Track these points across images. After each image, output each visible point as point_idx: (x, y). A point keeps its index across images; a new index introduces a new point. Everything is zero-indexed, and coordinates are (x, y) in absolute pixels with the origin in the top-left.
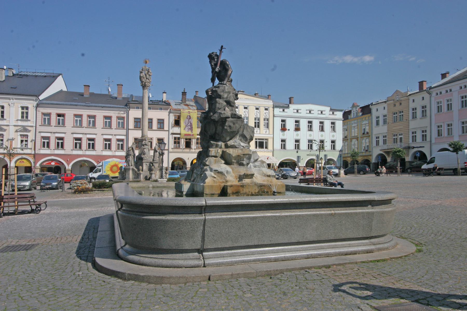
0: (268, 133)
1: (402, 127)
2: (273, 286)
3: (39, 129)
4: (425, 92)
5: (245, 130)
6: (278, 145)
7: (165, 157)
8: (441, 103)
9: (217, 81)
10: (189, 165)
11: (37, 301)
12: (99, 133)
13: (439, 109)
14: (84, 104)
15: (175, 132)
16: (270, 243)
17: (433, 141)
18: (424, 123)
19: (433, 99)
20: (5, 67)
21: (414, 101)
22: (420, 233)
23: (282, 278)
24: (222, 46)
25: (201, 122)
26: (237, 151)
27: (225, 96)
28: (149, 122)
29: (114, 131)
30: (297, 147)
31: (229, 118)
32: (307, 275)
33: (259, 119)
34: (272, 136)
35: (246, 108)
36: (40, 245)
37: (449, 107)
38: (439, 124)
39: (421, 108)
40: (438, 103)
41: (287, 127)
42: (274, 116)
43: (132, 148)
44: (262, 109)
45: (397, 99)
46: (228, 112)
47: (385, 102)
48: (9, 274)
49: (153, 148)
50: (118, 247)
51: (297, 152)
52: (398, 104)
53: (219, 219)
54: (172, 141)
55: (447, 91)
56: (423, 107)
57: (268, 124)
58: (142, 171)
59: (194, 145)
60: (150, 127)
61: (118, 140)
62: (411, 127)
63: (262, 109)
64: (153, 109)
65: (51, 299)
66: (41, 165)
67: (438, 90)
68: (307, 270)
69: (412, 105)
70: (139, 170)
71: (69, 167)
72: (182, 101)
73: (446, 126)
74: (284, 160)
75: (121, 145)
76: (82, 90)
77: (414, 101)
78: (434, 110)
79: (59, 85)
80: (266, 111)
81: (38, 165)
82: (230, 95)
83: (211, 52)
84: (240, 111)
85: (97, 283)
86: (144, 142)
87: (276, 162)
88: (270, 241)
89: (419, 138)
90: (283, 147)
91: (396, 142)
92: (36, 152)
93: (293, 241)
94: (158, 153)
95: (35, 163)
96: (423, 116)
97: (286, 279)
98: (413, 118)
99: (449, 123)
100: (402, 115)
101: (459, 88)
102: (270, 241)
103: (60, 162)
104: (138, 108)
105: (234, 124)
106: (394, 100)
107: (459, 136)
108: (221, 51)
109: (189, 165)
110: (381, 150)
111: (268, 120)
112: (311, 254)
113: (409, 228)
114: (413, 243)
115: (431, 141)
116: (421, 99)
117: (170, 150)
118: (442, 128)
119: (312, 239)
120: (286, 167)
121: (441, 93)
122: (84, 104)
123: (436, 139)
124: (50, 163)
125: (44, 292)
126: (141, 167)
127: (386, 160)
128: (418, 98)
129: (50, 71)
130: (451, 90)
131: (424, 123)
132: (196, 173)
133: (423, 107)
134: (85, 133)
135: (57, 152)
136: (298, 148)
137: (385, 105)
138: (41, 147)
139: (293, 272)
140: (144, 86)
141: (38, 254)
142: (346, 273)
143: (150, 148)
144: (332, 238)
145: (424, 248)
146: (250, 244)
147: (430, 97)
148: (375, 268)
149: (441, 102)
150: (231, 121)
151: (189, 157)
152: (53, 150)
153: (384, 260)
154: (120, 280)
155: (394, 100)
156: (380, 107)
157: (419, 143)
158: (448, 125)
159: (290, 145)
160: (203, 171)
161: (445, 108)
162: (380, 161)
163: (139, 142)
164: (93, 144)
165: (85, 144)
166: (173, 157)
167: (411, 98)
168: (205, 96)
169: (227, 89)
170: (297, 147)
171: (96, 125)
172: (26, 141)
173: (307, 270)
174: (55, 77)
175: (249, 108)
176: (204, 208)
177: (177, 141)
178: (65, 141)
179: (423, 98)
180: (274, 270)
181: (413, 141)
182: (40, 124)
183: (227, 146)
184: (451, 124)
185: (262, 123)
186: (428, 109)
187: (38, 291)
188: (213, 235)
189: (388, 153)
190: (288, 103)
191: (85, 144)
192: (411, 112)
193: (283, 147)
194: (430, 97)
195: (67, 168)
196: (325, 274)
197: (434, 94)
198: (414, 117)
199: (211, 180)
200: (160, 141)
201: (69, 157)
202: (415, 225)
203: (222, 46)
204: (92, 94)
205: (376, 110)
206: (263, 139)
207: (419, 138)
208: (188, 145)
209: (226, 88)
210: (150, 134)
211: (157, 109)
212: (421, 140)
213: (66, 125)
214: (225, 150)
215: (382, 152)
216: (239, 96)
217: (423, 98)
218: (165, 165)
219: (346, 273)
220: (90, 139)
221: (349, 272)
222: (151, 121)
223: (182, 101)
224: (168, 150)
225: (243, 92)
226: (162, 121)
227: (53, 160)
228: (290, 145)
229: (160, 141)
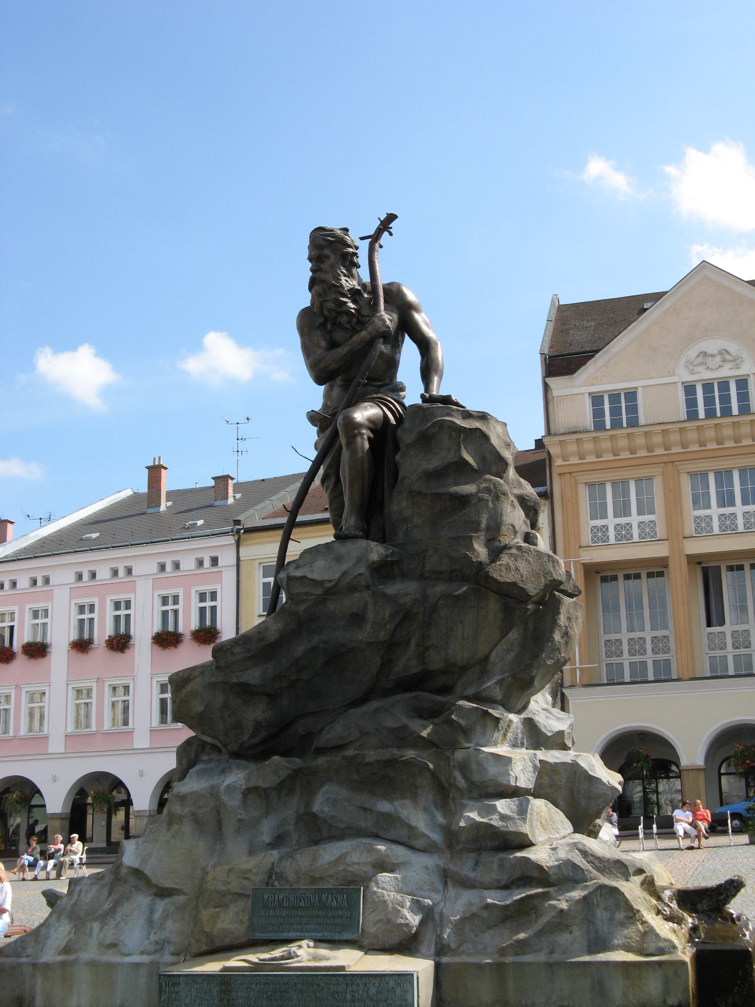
101: (154, 568)
130: (47, 580)
149: (12, 614)
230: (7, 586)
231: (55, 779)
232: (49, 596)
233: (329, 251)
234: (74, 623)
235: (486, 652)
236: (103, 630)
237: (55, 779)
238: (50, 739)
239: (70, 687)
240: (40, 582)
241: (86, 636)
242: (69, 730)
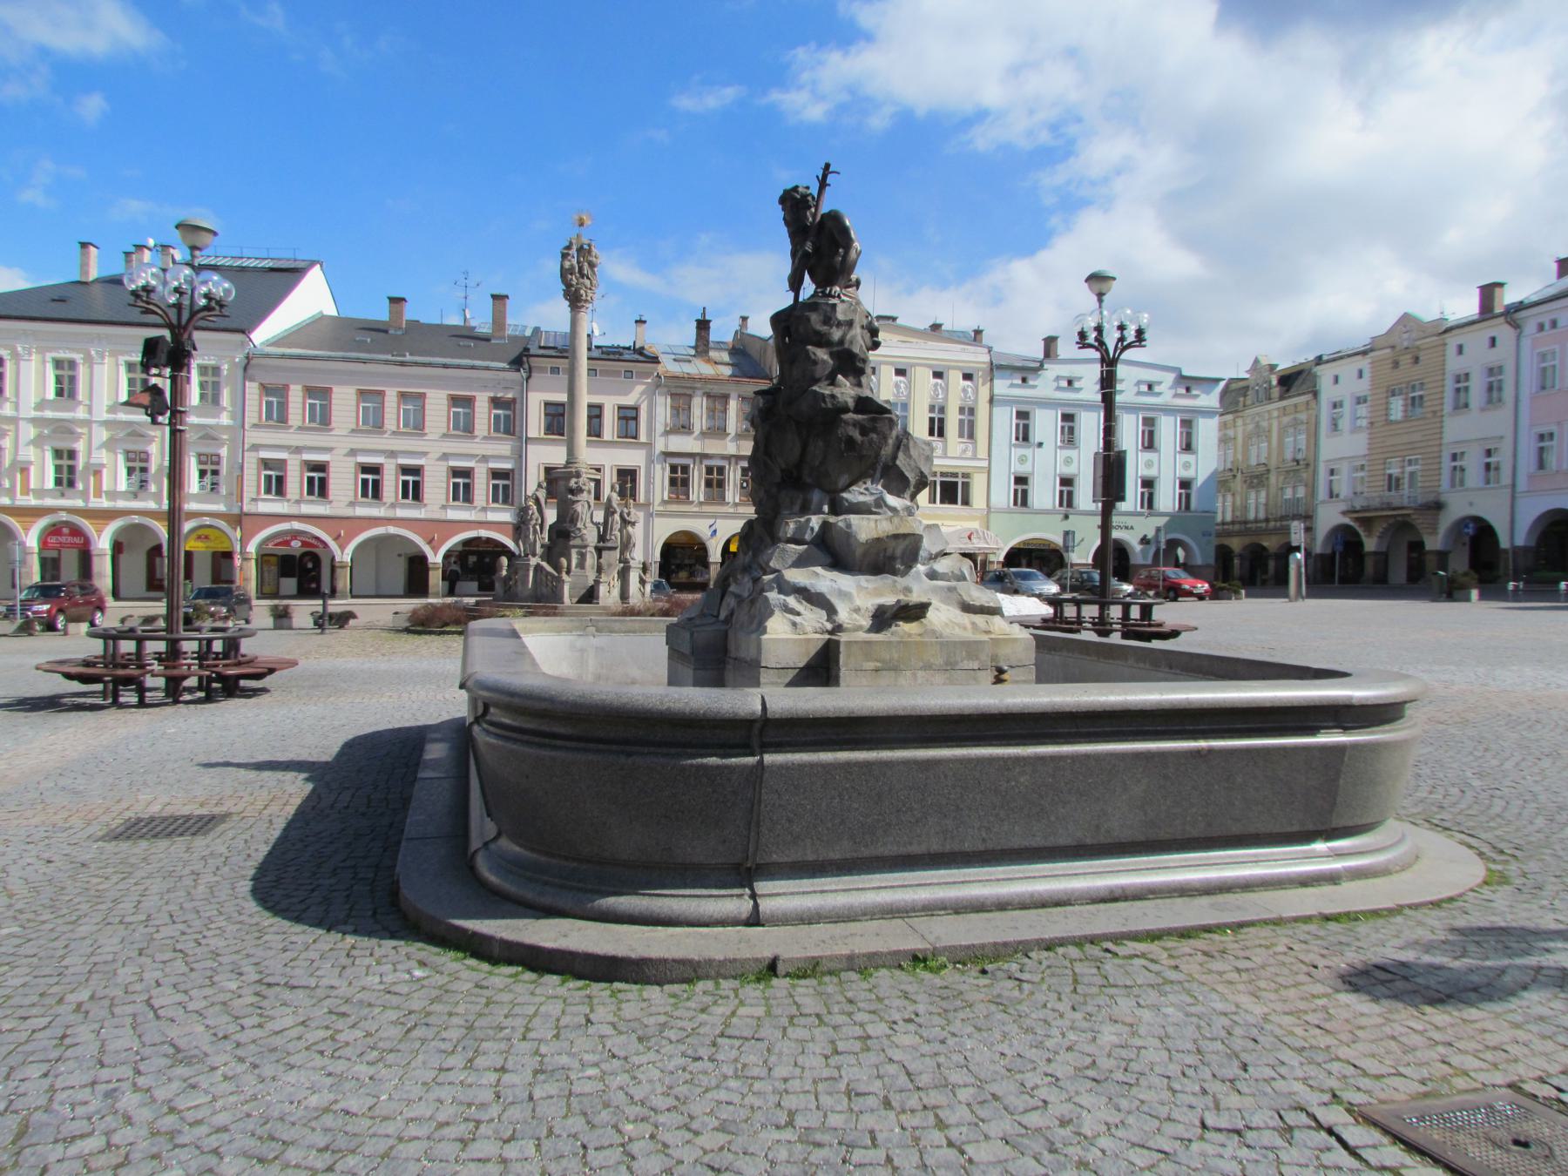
0: (969, 454)
1: (1416, 437)
2: (993, 1008)
3: (253, 437)
4: (1502, 319)
5: (901, 455)
6: (1003, 494)
7: (637, 532)
9: (808, 288)
10: (715, 555)
11: (202, 1028)
12: (435, 452)
14: (389, 357)
15: (672, 449)
16: (982, 848)
17: (1522, 484)
18: (1497, 423)
19: (1526, 343)
20: (151, 243)
21: (1460, 349)
22: (1497, 809)
23: (1025, 976)
24: (827, 166)
25: (753, 424)
26: (872, 524)
27: (836, 334)
28: (590, 417)
29: (477, 447)
30: (1067, 499)
31: (846, 410)
32: (1110, 966)
33: (942, 410)
34: (985, 464)
35: (900, 372)
36: (235, 818)
38: (1544, 430)
40: (1543, 357)
41: (1037, 434)
42: (991, 401)
43: (537, 501)
44: (955, 378)
45: (1406, 344)
46: (845, 390)
47: (1364, 353)
48: (127, 919)
49: (604, 499)
50: (475, 843)
51: (1066, 517)
52: (1406, 360)
53: (812, 765)
54: (661, 475)
56: (1491, 371)
57: (972, 425)
58: (568, 572)
59: (732, 493)
60: (595, 431)
61: (496, 474)
63: (955, 378)
64: (606, 373)
65: (247, 1022)
66: (260, 546)
67: (1544, 314)
68: (1109, 945)
69: (1454, 364)
70: (557, 568)
71: (345, 556)
72: (695, 348)
74: (1024, 542)
75: (505, 483)
76: (381, 313)
77: (1460, 349)
79: (311, 299)
80: (968, 383)
81: (252, 548)
82: (852, 333)
83: (789, 187)
84: (884, 388)
85: (399, 967)
86: (573, 481)
87: (998, 546)
88: (984, 840)
89: (1474, 476)
90: (1022, 499)
91: (1398, 486)
92: (246, 509)
93: (1063, 840)
94: (617, 517)
95: (244, 542)
96: (1490, 401)
97: (1037, 978)
98: (1456, 408)
100: (1421, 397)
102: (984, 840)
103: (317, 538)
104: (555, 370)
105: (864, 432)
106: (1393, 347)
108: (823, 184)
109: (715, 555)
110: (1344, 513)
111: (972, 411)
112: (1123, 888)
113: (1454, 791)
114: (1470, 847)
115: (1514, 486)
116: (1487, 342)
117: (657, 507)
118: (1554, 443)
119: (1125, 835)
120: (1029, 566)
122: (389, 357)
124: (287, 543)
125: (229, 995)
126: (564, 561)
127: (1360, 544)
128: (1476, 341)
129: (282, 254)
131: (1497, 423)
132: (737, 596)
133: (1491, 371)
134: (390, 448)
135: (306, 509)
136: (1070, 504)
137: (1364, 363)
138: (259, 492)
139: (1061, 950)
140: (575, 300)
141: (223, 849)
142: (1248, 964)
143: (592, 501)
144: (1195, 833)
145: (1513, 867)
146: (915, 849)
147: (1518, 338)
148: (1348, 945)
149: (1554, 353)
150: (855, 424)
151: (720, 525)
152: (296, 503)
153: (1375, 913)
154: (473, 962)
155: (1393, 347)
156: (1347, 370)
157: (1473, 490)
159: (1044, 494)
160: (759, 590)
162: (1340, 548)
163: (558, 483)
164: (417, 485)
165: (391, 484)
166: (664, 529)
167: (1452, 341)
168: (766, 331)
169: (844, 313)
170: (1067, 499)
171: (427, 424)
172: (215, 473)
173: (1109, 945)
174: (288, 275)
175: (911, 372)
176: (758, 725)
177: (679, 481)
178: (332, 475)
179: (1493, 342)
180: (995, 944)
181: (1453, 485)
182: (256, 421)
183: (835, 510)
185: (952, 421)
186: (1508, 379)
187: (209, 991)
188: (790, 821)
189: (1367, 522)
190: (1041, 356)
191: (391, 484)
192: (1450, 385)
193: (1022, 499)
194: (1518, 338)
195: (338, 559)
196: (1172, 962)
197: (1530, 328)
198: (1461, 406)
199: (786, 634)
200: (627, 477)
201: (343, 526)
202: (1476, 783)
203: (827, 166)
204: (414, 325)
205: (1332, 380)
206: (956, 475)
207: (1474, 476)
208: (715, 483)
209: (840, 308)
210: (588, 456)
211: (617, 373)
213: (333, 425)
214: (832, 519)
215: (1346, 520)
216: (881, 336)
217: (1493, 342)
218: (637, 556)
219: (1248, 964)
220: (406, 470)
221: (1259, 957)
222: (596, 413)
223: (695, 348)
224: (647, 505)
225: (1541, 465)
226: (632, 414)
227: (296, 534)
228: (1044, 494)
229: (627, 477)
233: (795, 204)
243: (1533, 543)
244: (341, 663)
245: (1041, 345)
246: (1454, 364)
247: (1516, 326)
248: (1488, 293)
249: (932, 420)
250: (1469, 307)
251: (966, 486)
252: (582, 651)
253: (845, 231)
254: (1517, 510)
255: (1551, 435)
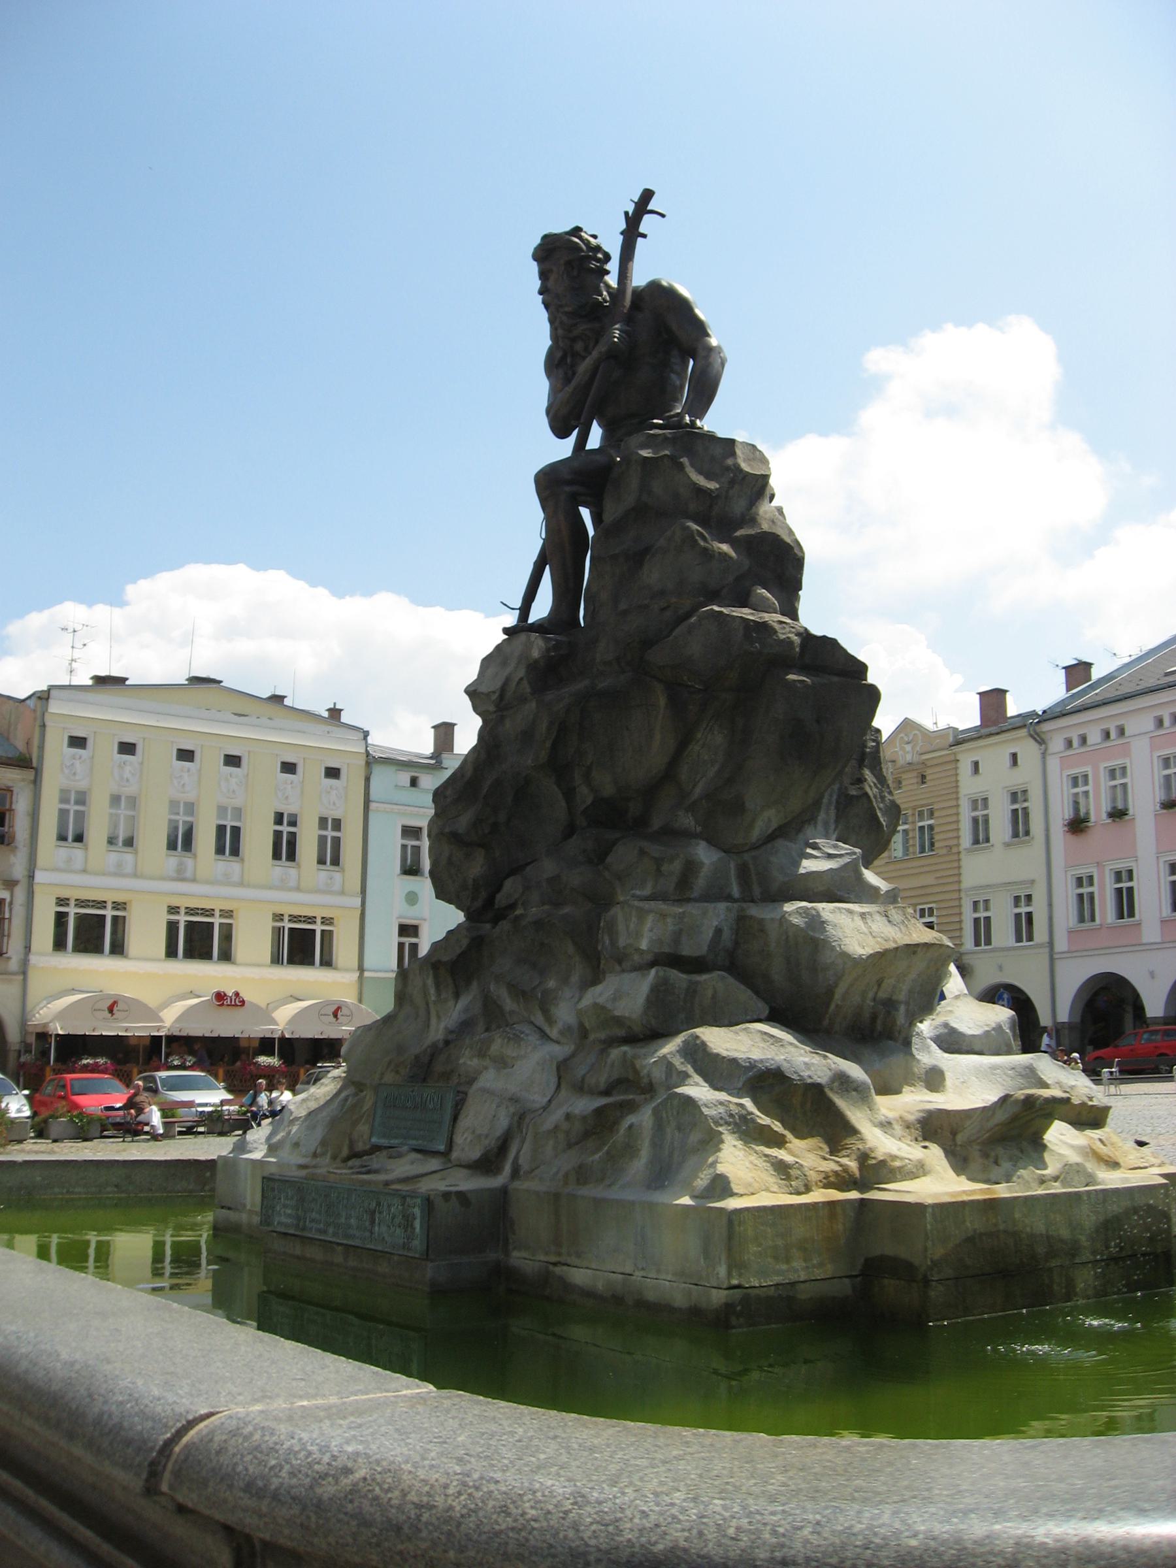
1: (929, 880)
8: (1086, 783)
13: (1085, 906)
17: (1061, 944)
19: (1053, 764)
21: (976, 765)
24: (647, 195)
37: (1125, 903)
38: (1083, 871)
39: (1007, 799)
55: (1107, 735)
62: (968, 881)
63: (312, 772)
73: (1103, 776)
77: (976, 765)
78: (1065, 914)
89: (1003, 933)
98: (976, 841)
99: (1121, 865)
100: (931, 827)
101: (1150, 725)
107: (1163, 922)
108: (631, 233)
115: (1051, 944)
116: (1007, 760)
121: (1083, 740)
123: (1070, 932)
128: (994, 756)
130: (1121, 731)
133: (1014, 797)
147: (1044, 755)
149: (1086, 776)
158: (1112, 773)
161: (1106, 909)
181: (977, 944)
184: (1130, 872)
194: (1044, 755)
197: (1056, 744)
203: (647, 195)
207: (1003, 933)
212: (1011, 941)
230: (1167, 722)
231: (1152, 974)
232: (1126, 751)
233: (566, 264)
234: (1158, 781)
235: (465, 1171)
236: (1098, 810)
237: (1152, 974)
238: (7, 1251)
239: (1162, 860)
240: (1075, 743)
241: (1120, 806)
242: (1164, 915)
243: (1077, 1019)
244: (658, 737)
245: (430, 736)
246: (969, 786)
247: (1040, 739)
248: (993, 700)
249: (278, 835)
250: (969, 717)
251: (327, 936)
252: (1025, 801)
253: (682, 307)
254: (1047, 974)
255: (1091, 878)
